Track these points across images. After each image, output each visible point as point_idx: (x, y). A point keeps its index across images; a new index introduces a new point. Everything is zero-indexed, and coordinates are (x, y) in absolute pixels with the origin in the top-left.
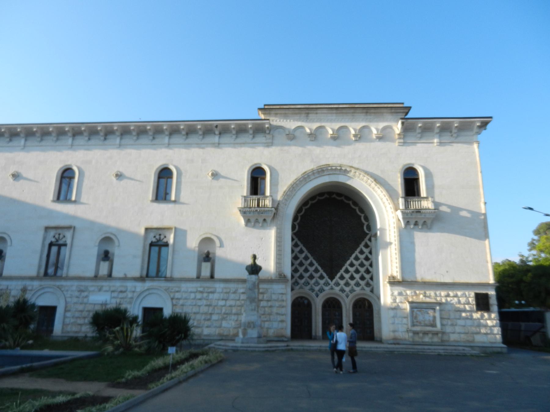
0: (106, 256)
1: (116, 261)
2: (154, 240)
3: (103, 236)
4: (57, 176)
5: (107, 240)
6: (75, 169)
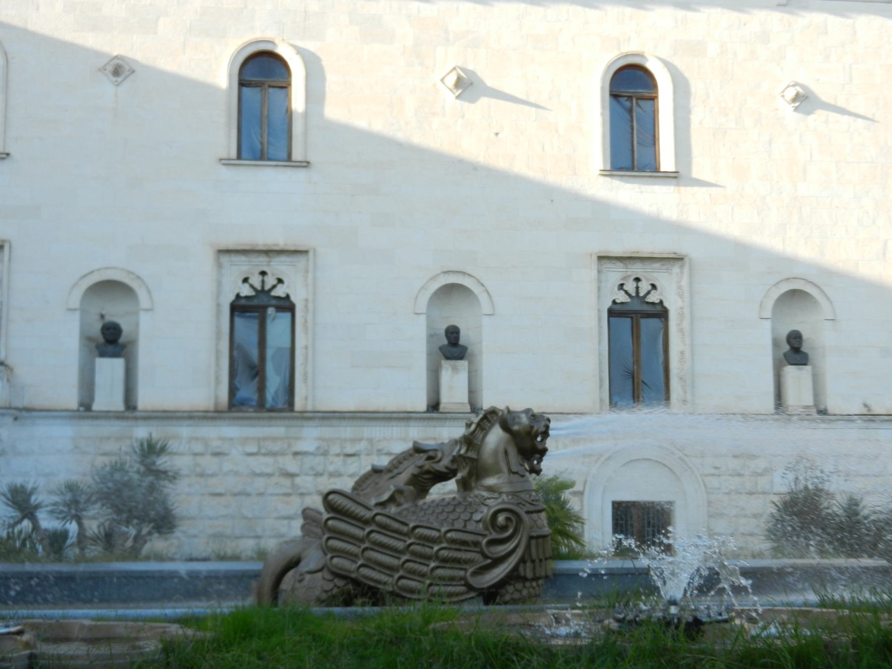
0: (111, 340)
1: (147, 353)
2: (246, 291)
3: (785, 288)
4: (603, 88)
5: (795, 297)
6: (653, 66)
